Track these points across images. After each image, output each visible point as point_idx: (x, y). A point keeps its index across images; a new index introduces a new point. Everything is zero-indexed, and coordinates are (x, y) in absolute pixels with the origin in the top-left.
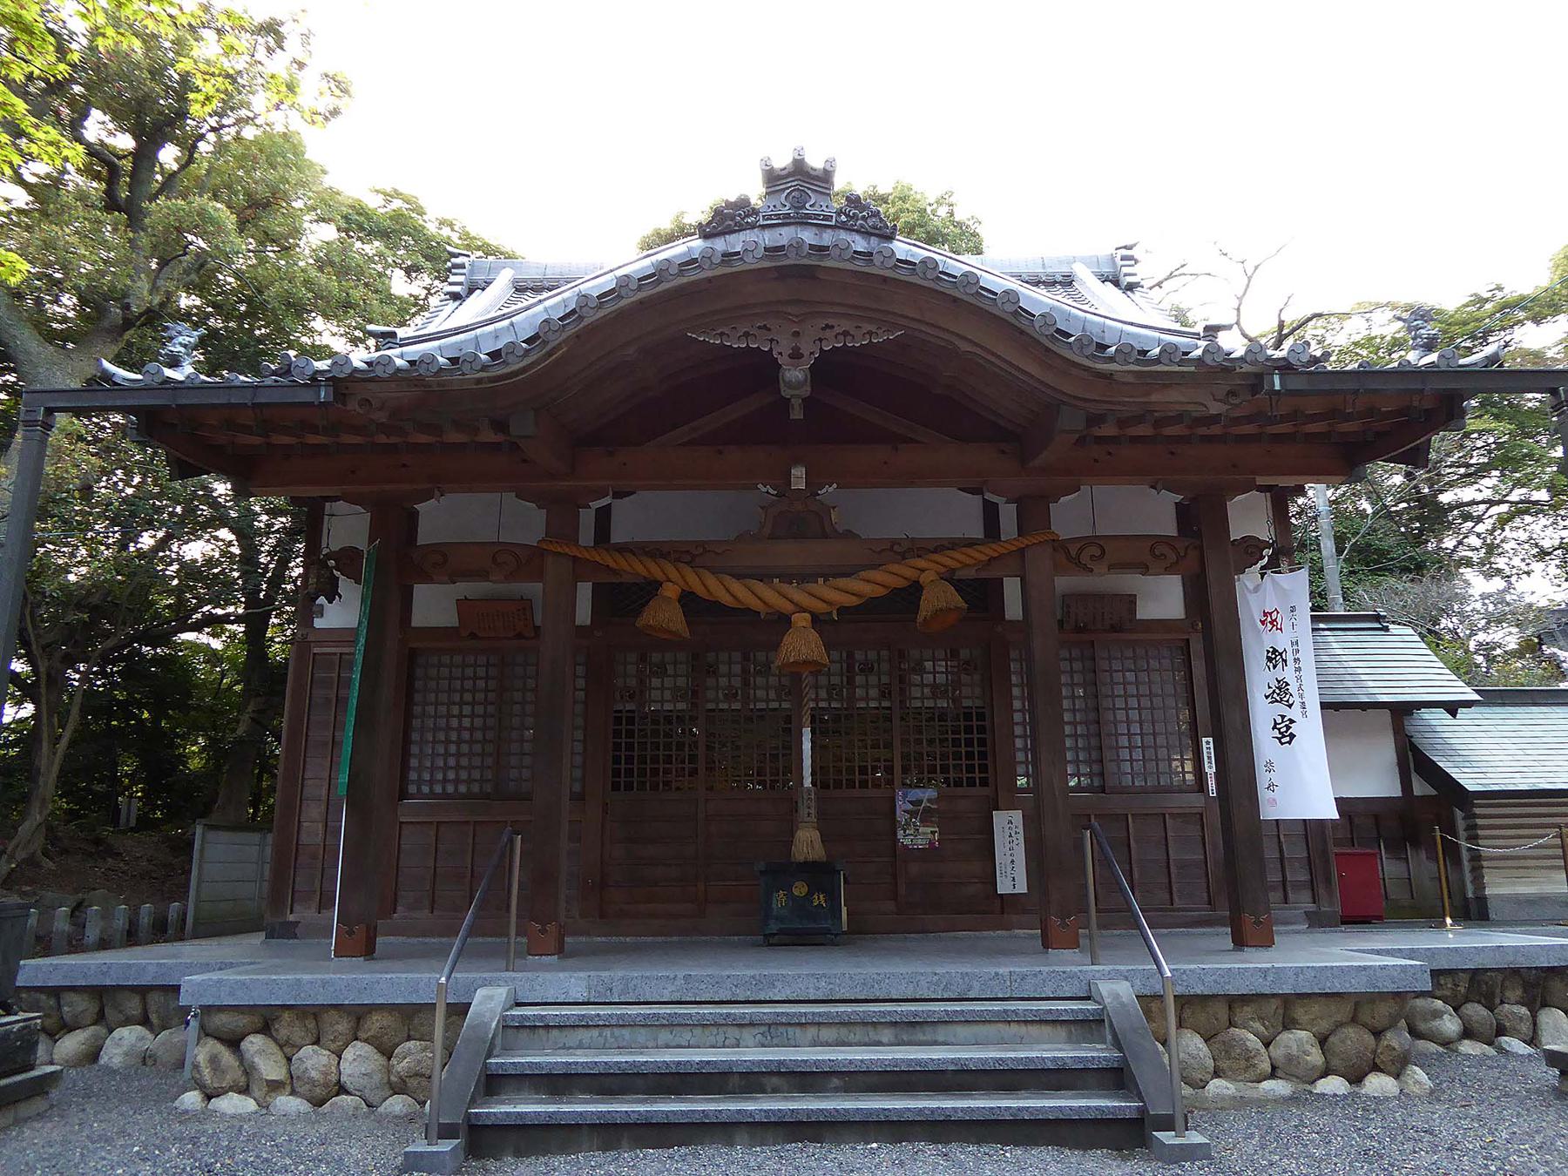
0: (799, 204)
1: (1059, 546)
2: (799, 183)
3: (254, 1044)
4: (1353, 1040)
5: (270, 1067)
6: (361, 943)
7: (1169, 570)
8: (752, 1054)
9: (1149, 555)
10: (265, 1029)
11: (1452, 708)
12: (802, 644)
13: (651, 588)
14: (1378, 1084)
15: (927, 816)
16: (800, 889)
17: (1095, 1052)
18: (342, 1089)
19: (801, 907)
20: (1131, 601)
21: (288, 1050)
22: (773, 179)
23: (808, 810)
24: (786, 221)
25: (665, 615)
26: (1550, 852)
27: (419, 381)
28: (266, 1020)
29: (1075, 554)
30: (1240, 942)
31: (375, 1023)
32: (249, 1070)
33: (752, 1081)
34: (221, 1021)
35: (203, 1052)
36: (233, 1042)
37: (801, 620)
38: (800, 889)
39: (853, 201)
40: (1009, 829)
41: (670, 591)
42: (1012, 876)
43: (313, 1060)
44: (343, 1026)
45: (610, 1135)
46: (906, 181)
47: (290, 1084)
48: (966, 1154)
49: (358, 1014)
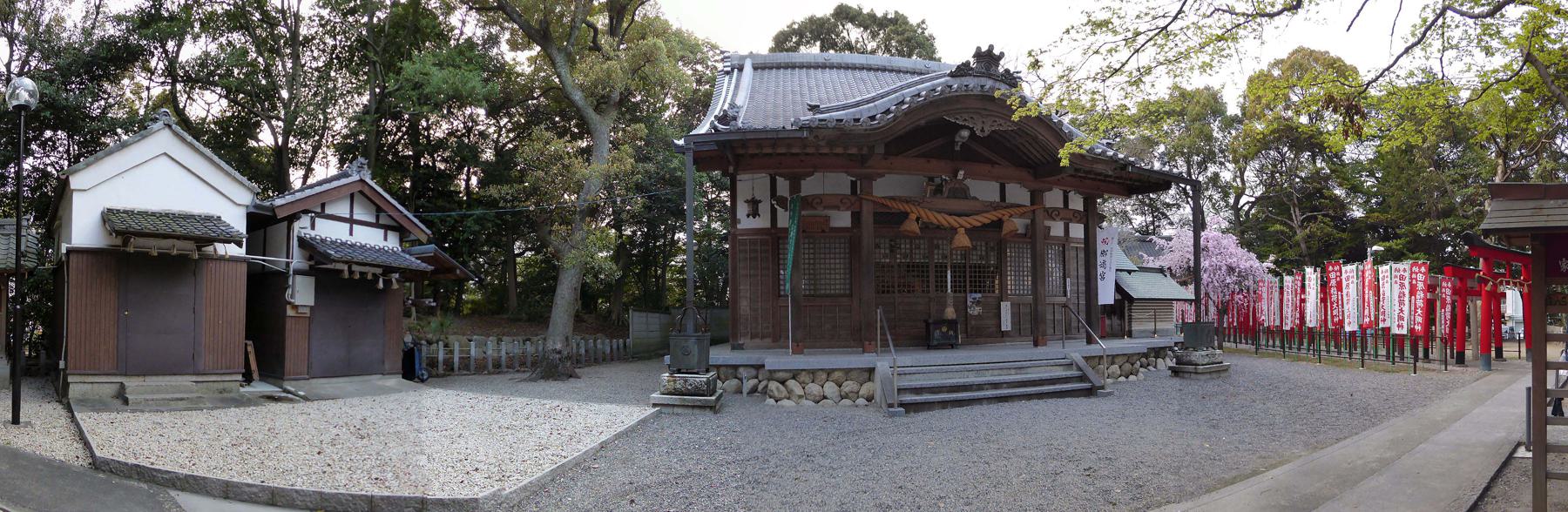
0: (988, 69)
1: (1046, 210)
2: (988, 59)
3: (791, 383)
4: (1127, 366)
5: (798, 390)
6: (798, 350)
7: (1079, 222)
8: (972, 379)
9: (838, 203)
10: (794, 378)
11: (1129, 272)
12: (962, 240)
13: (906, 215)
14: (1132, 378)
15: (978, 303)
16: (944, 329)
17: (1074, 372)
18: (825, 397)
19: (944, 335)
20: (827, 219)
21: (803, 385)
22: (979, 55)
23: (950, 301)
24: (982, 75)
25: (912, 226)
26: (1288, 311)
27: (840, 129)
28: (795, 375)
29: (807, 202)
30: (1036, 344)
31: (837, 375)
32: (790, 392)
33: (980, 387)
34: (781, 375)
35: (773, 385)
36: (783, 383)
37: (962, 230)
38: (944, 329)
39: (1007, 71)
40: (1006, 308)
41: (913, 217)
42: (1006, 325)
43: (814, 388)
44: (824, 376)
45: (944, 404)
46: (774, 33)
47: (805, 396)
48: (1061, 401)
49: (829, 372)
